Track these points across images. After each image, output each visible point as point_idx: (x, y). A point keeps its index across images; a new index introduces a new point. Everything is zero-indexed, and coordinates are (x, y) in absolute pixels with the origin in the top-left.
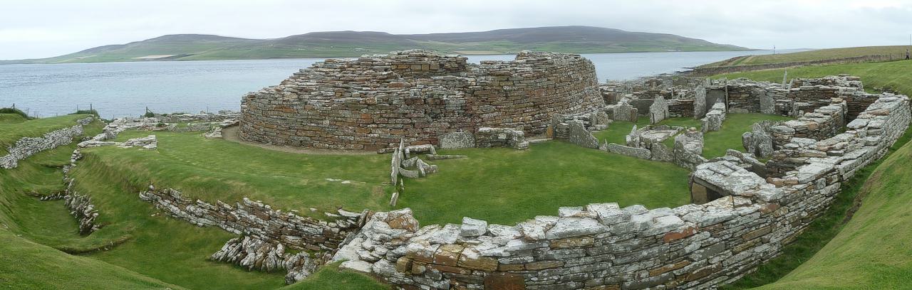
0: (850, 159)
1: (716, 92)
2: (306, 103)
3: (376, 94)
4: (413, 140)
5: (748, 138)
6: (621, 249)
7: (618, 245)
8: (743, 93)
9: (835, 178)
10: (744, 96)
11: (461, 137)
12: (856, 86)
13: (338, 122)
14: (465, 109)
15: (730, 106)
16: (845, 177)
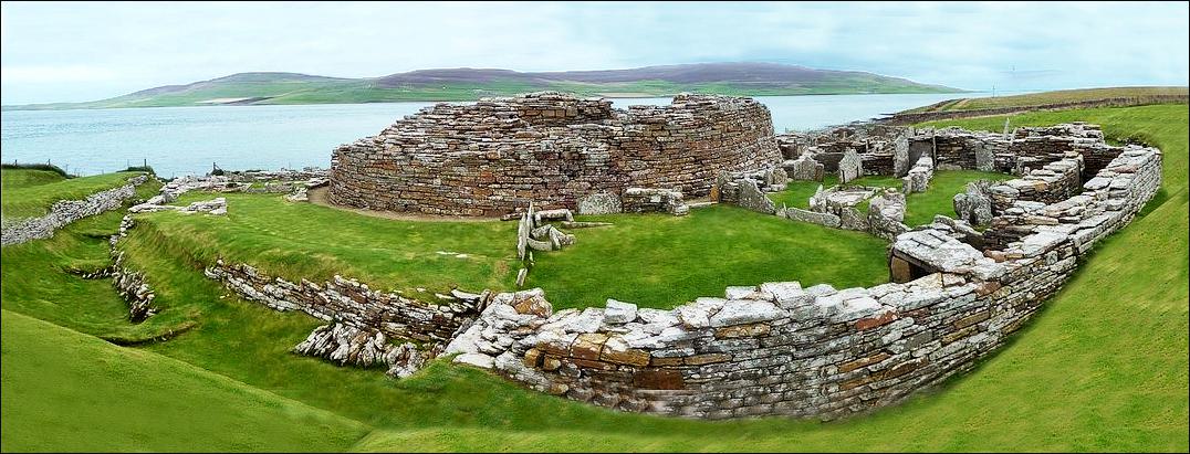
3: (499, 147)
4: (545, 203)
8: (955, 146)
11: (604, 200)
12: (1095, 137)
13: (453, 182)
14: (610, 165)
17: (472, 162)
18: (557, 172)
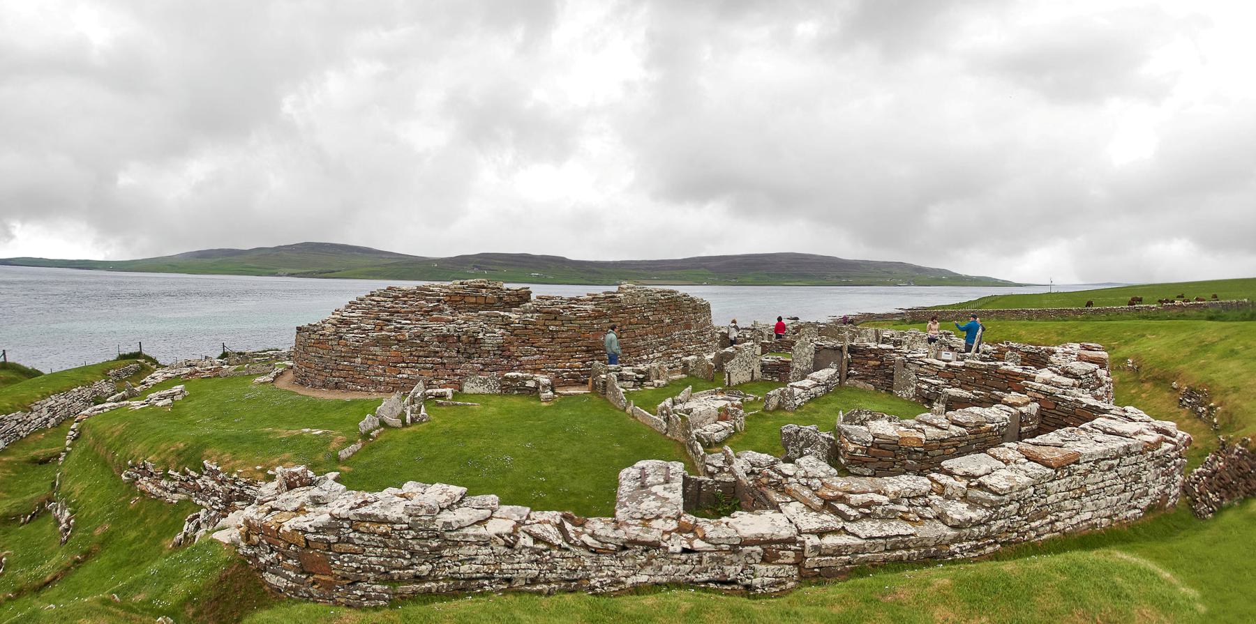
0: (854, 534)
1: (831, 353)
2: (341, 338)
3: (411, 328)
4: (442, 382)
5: (789, 434)
6: (417, 547)
7: (414, 542)
8: (871, 359)
9: (790, 556)
10: (872, 363)
11: (485, 382)
12: (1076, 377)
13: (370, 360)
14: (502, 350)
15: (848, 376)
16: (808, 563)
17: (384, 342)
18: (454, 353)
